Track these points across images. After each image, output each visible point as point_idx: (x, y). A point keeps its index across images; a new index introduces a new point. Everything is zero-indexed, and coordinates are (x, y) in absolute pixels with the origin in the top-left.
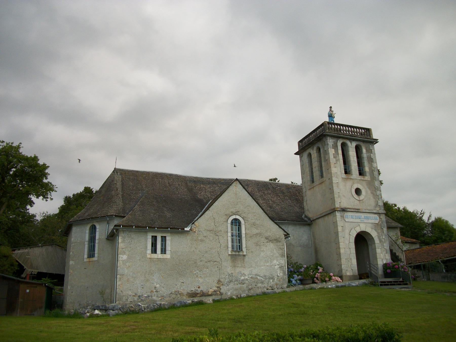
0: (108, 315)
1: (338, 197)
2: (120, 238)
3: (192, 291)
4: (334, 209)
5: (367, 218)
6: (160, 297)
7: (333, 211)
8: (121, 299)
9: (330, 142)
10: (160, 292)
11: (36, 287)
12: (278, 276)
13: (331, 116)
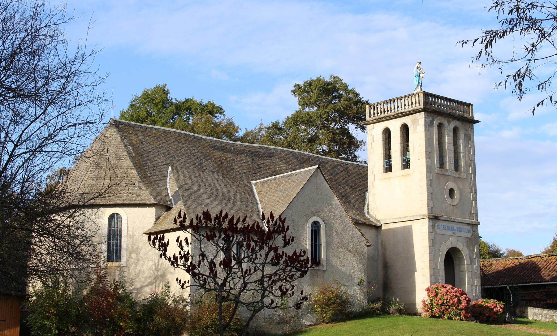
5: (460, 230)
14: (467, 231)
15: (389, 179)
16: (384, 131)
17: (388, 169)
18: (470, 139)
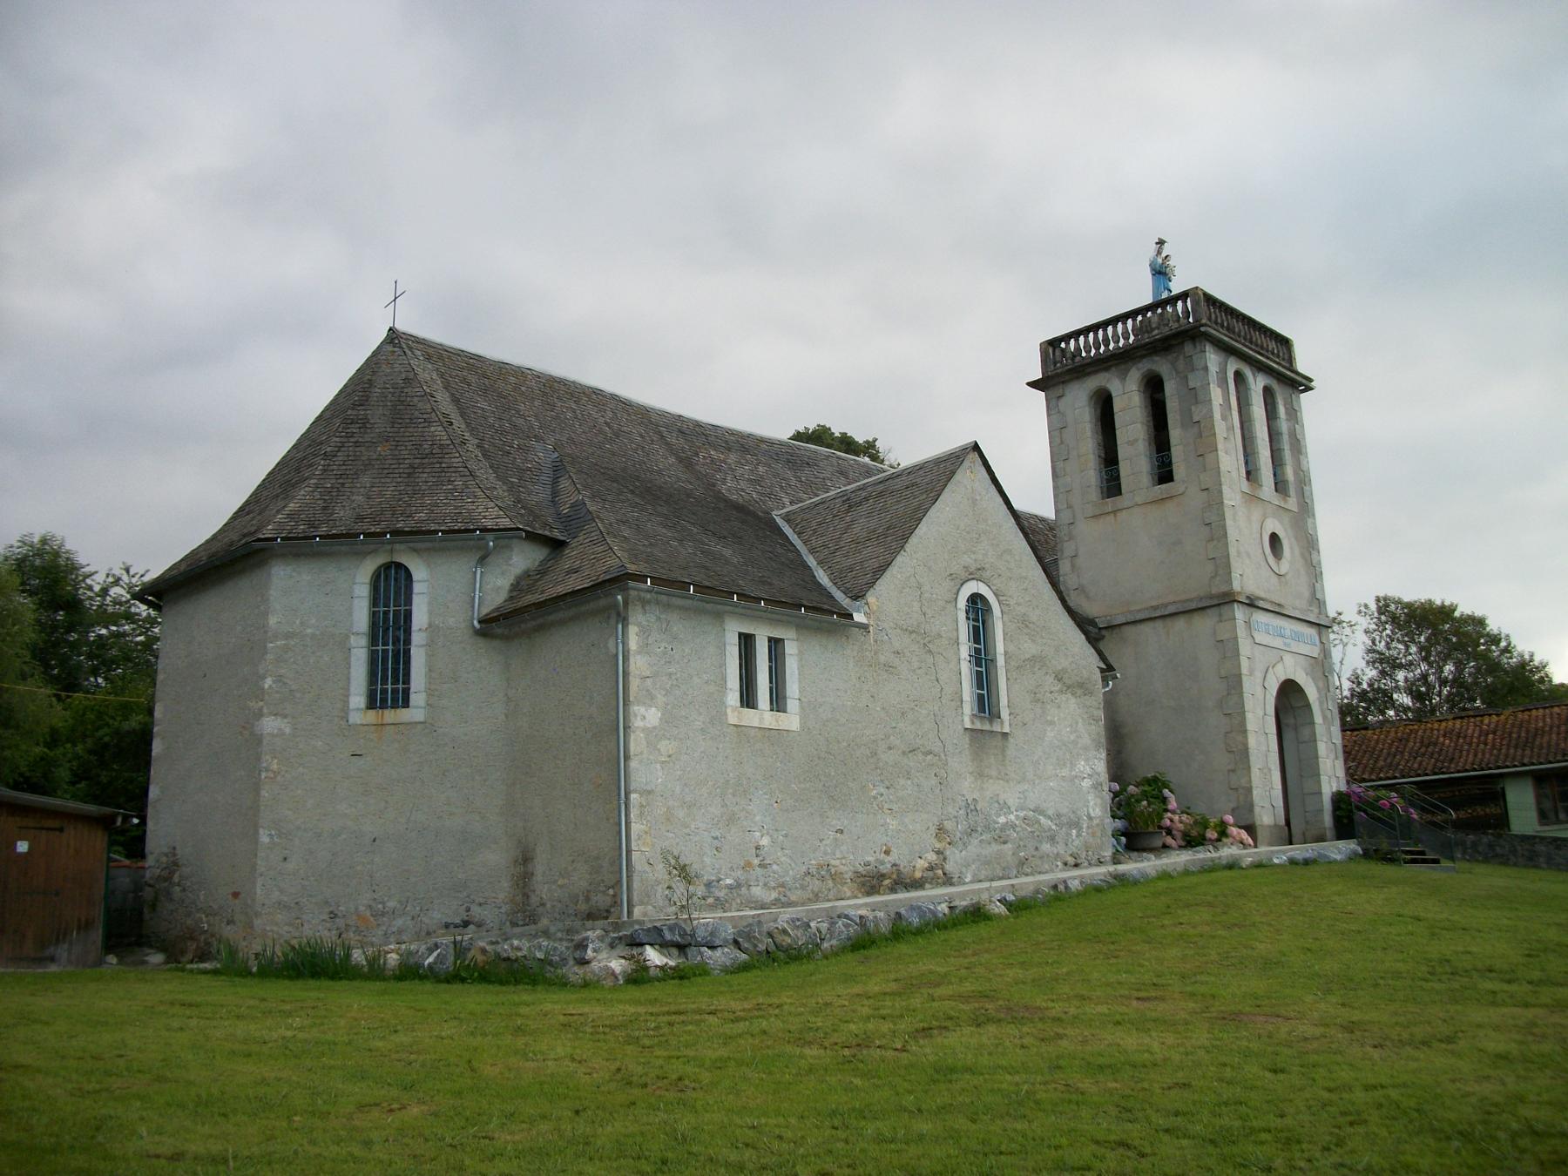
0: (702, 971)
2: (633, 630)
3: (867, 864)
4: (1225, 594)
5: (1297, 637)
6: (774, 888)
7: (1226, 600)
8: (649, 897)
9: (1212, 358)
10: (775, 867)
11: (61, 830)
12: (1090, 818)
13: (1161, 272)
15: (1115, 516)
16: (1091, 398)
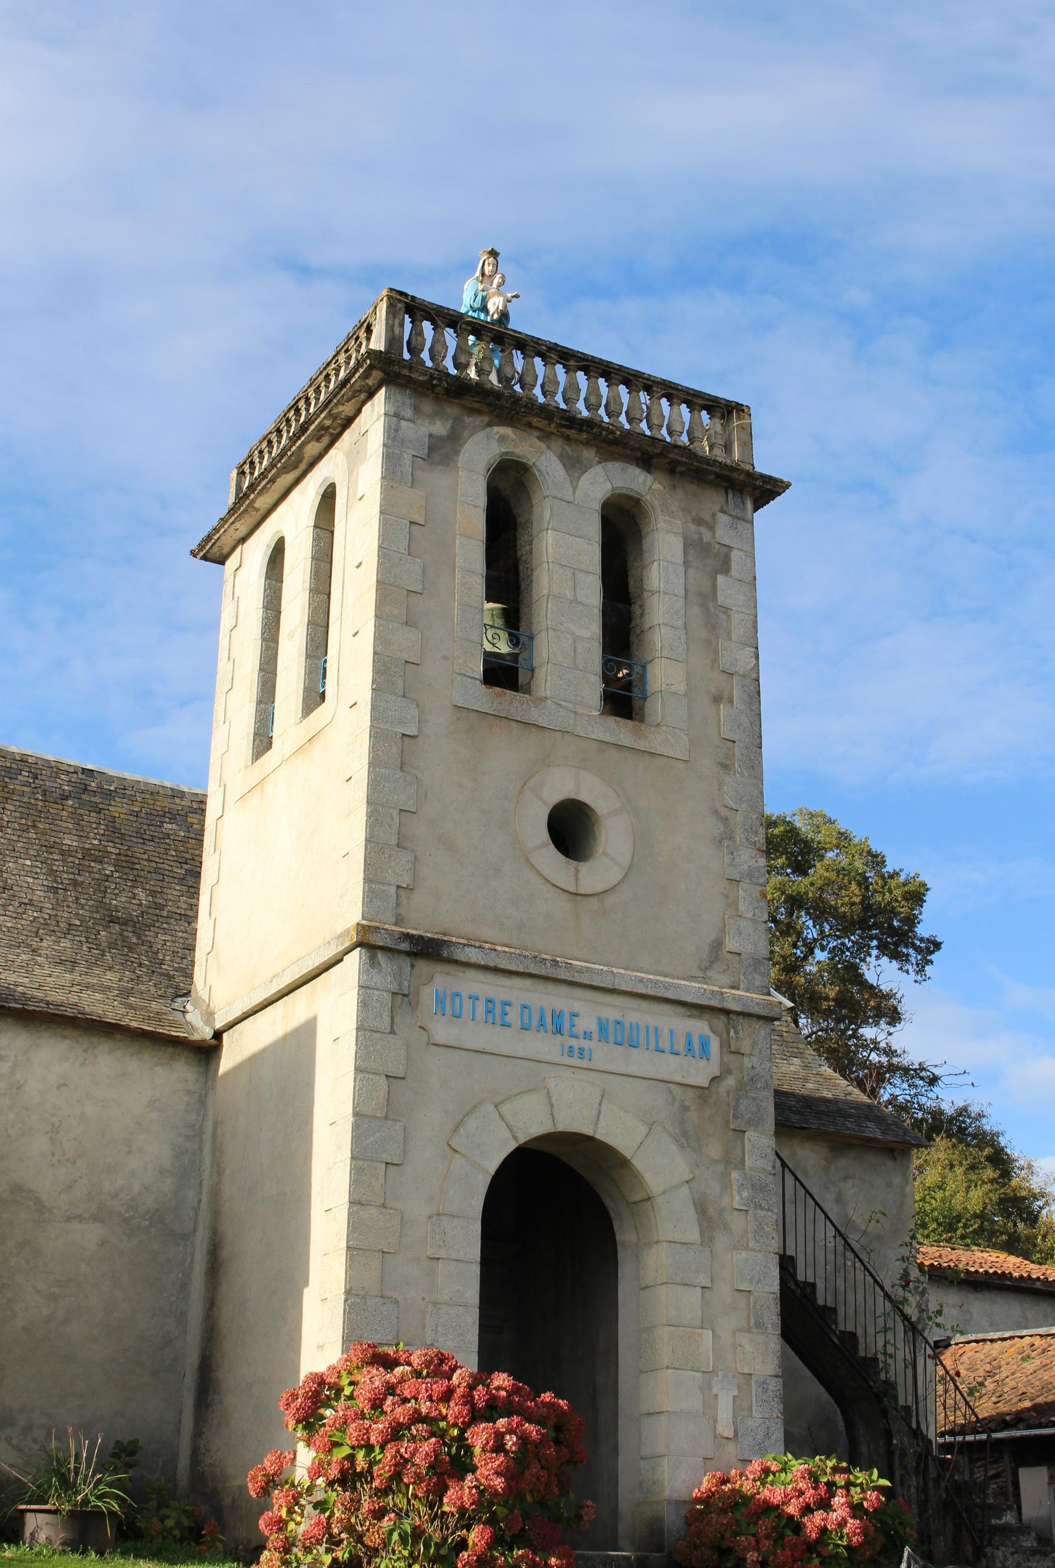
1: (394, 841)
14: (680, 1047)
17: (263, 742)
18: (725, 566)
